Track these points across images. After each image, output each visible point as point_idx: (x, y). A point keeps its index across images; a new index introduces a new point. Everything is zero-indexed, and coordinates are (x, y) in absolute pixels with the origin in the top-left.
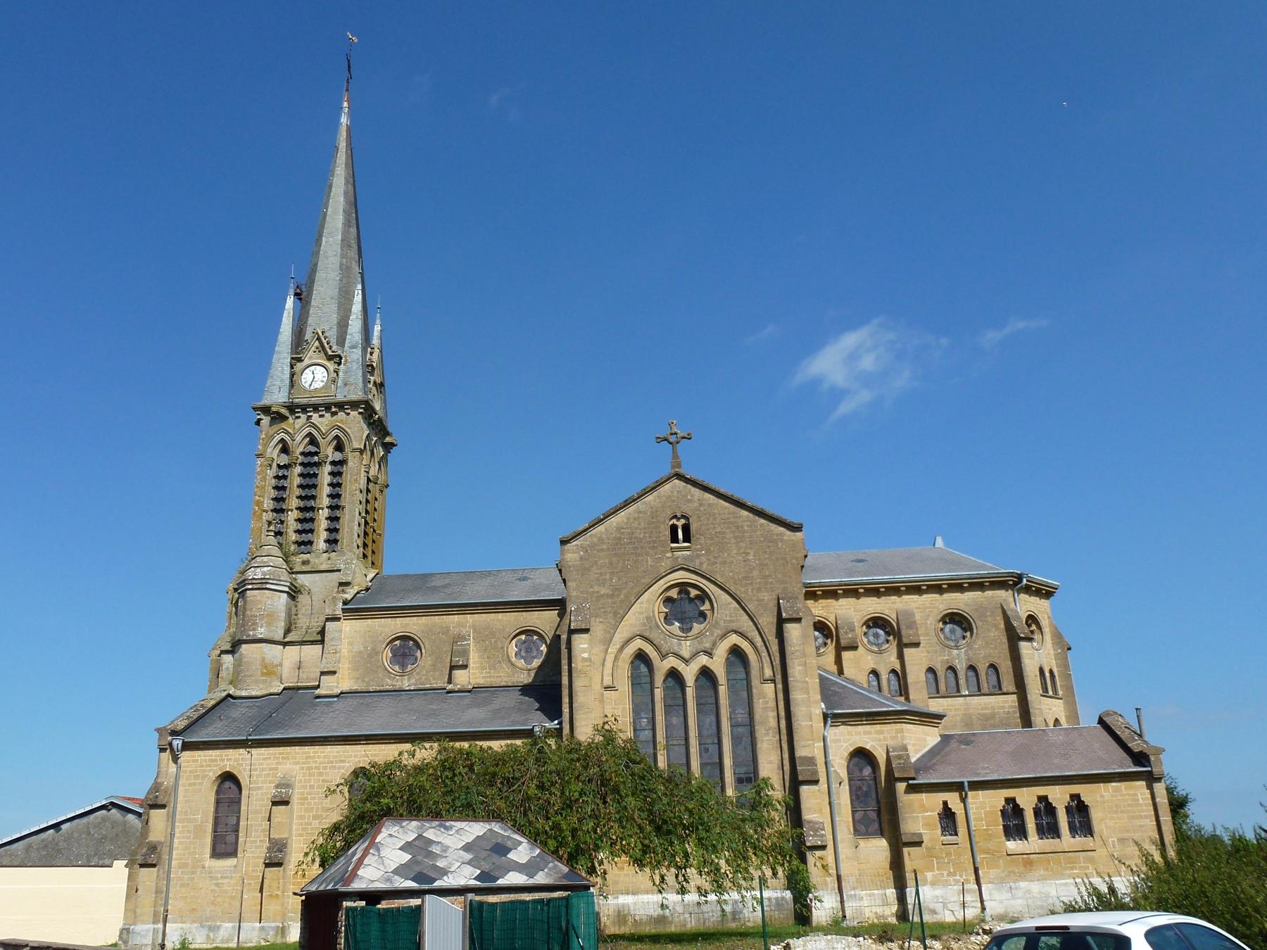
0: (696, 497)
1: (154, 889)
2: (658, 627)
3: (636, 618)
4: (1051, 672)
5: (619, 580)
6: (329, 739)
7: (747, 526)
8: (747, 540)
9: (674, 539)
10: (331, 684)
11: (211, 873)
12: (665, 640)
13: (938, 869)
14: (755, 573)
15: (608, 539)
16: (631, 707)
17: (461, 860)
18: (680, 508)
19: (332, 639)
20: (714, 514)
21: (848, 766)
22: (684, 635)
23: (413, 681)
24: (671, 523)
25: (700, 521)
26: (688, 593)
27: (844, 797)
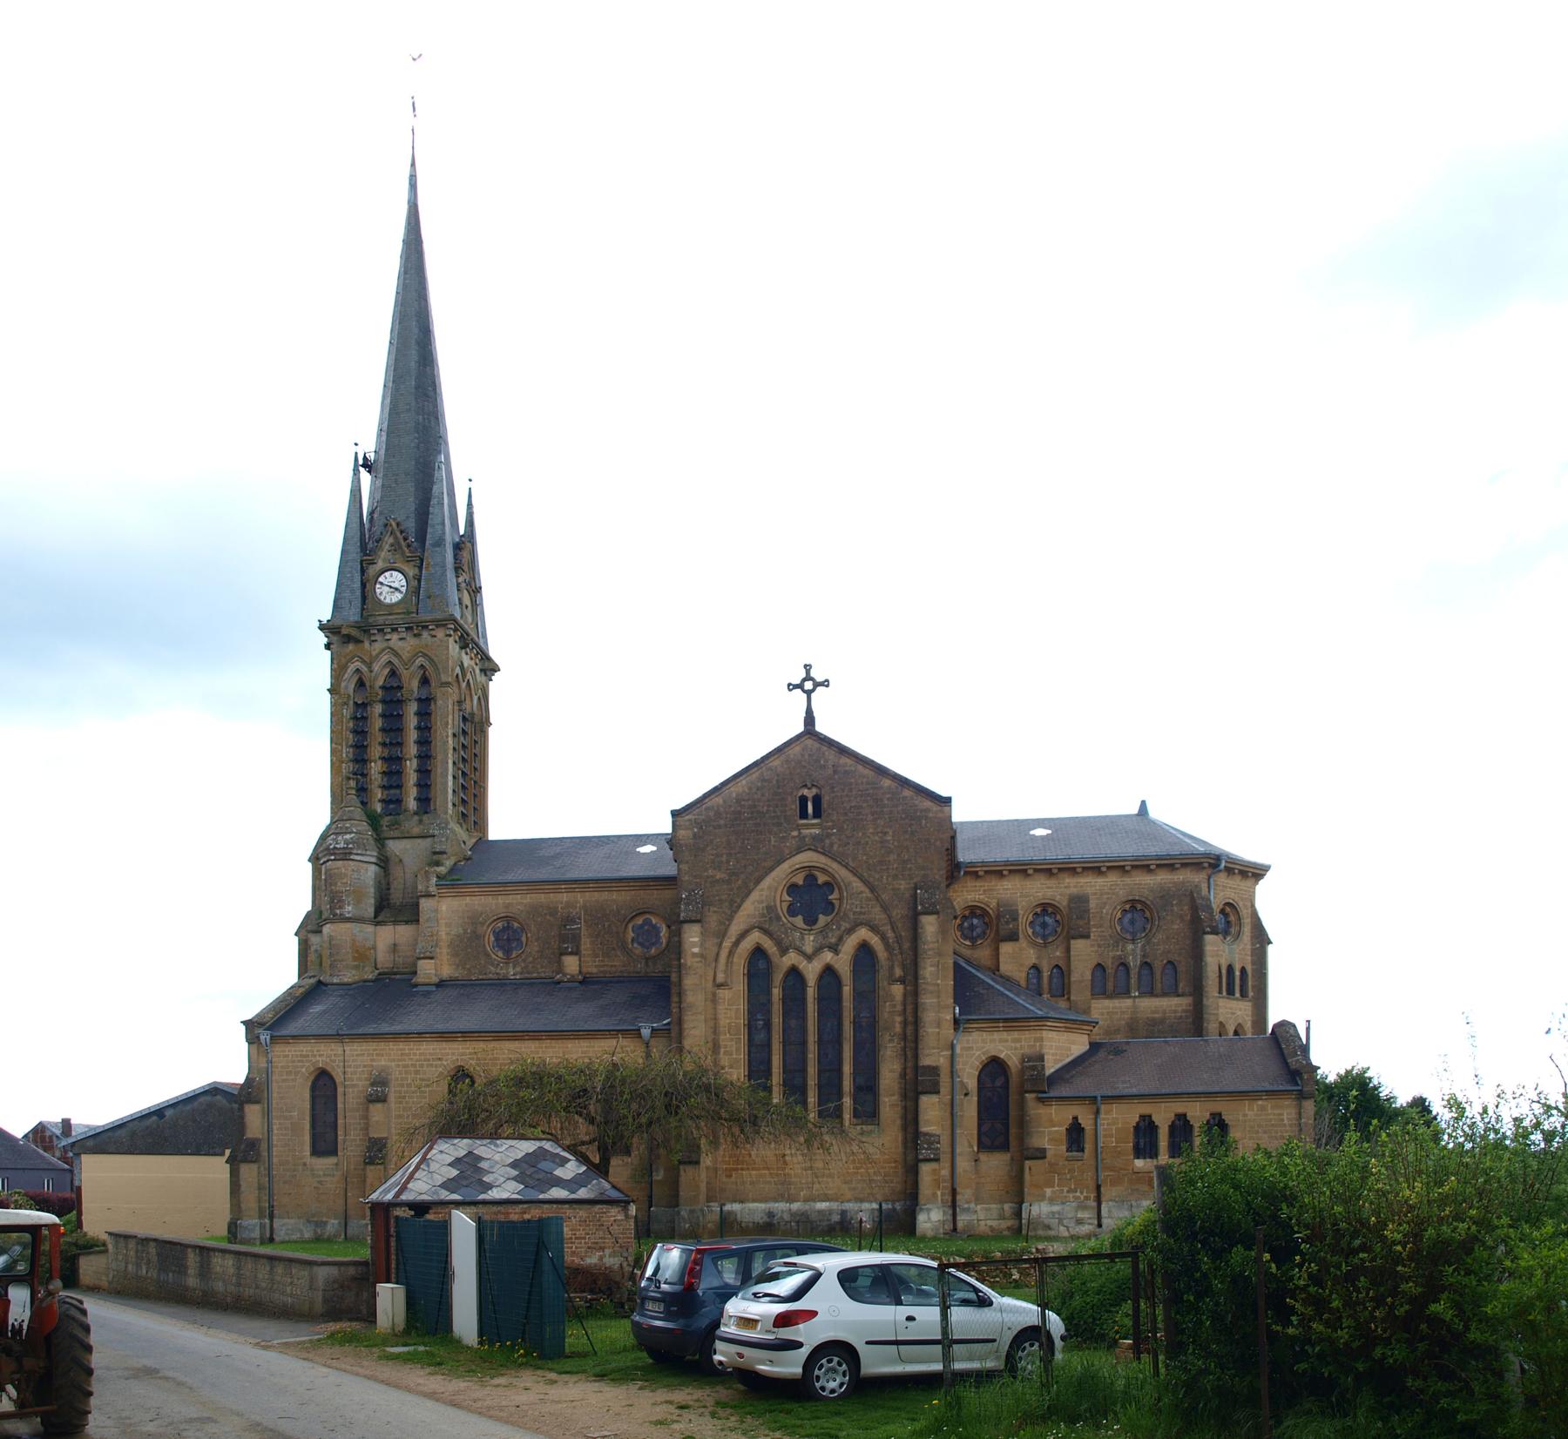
0: (830, 762)
1: (256, 1185)
2: (779, 919)
3: (755, 908)
4: (1243, 970)
5: (738, 862)
6: (424, 1035)
7: (888, 799)
8: (887, 816)
9: (804, 815)
10: (428, 972)
11: (312, 1170)
12: (786, 934)
13: (1058, 1186)
14: (892, 857)
15: (727, 814)
16: (746, 1008)
17: (506, 1176)
18: (810, 776)
19: (427, 920)
20: (851, 784)
21: (979, 1076)
22: (809, 928)
23: (518, 969)
24: (800, 794)
25: (834, 792)
26: (815, 878)
27: (969, 1110)
